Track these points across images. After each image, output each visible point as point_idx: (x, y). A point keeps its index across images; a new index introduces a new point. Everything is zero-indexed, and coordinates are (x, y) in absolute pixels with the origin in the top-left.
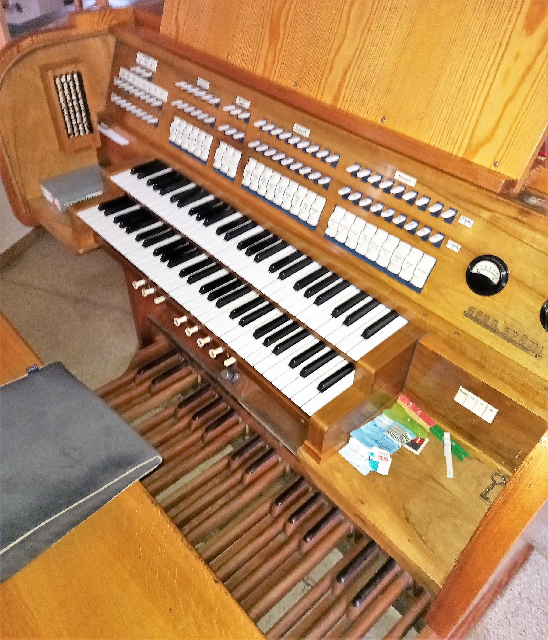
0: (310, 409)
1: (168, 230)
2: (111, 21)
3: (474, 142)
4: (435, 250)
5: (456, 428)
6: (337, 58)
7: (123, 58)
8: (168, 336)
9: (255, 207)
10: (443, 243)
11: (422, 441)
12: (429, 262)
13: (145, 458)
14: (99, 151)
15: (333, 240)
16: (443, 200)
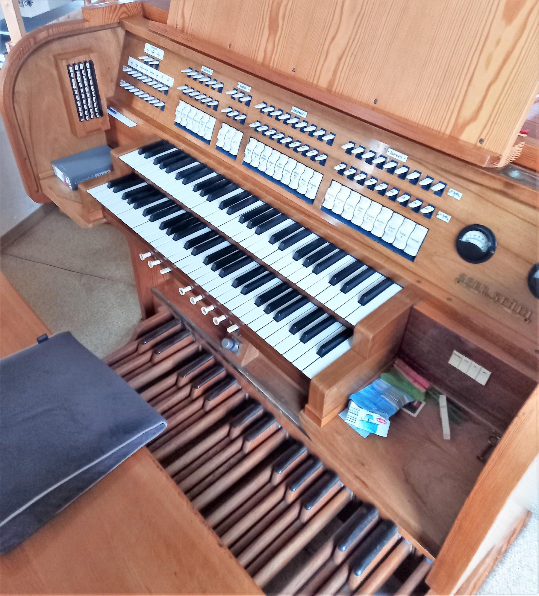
0: (309, 373)
1: (173, 205)
2: (121, 14)
3: (461, 121)
4: (426, 221)
5: (449, 389)
6: (331, 47)
7: (131, 46)
8: (169, 306)
9: (255, 183)
10: (434, 214)
11: (420, 403)
12: (421, 232)
13: (150, 422)
14: (107, 132)
15: (330, 212)
16: (432, 175)
